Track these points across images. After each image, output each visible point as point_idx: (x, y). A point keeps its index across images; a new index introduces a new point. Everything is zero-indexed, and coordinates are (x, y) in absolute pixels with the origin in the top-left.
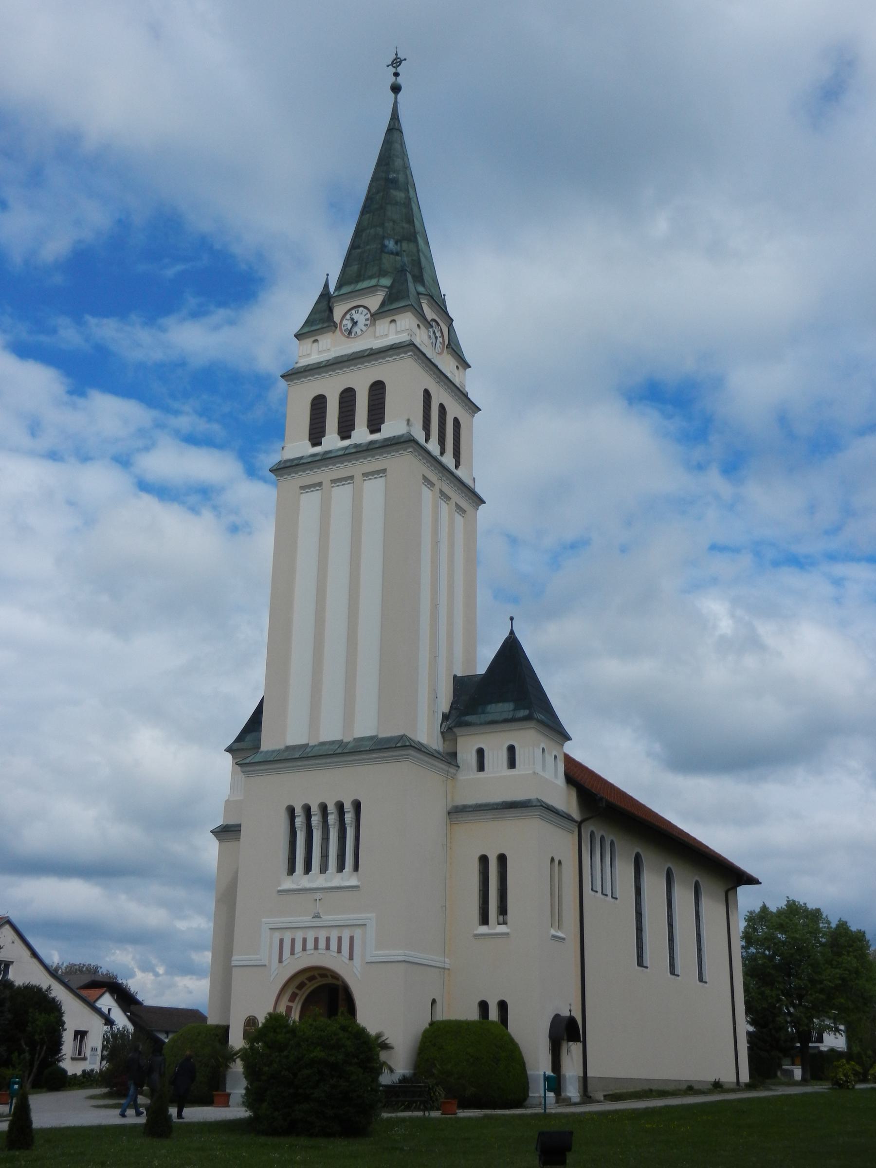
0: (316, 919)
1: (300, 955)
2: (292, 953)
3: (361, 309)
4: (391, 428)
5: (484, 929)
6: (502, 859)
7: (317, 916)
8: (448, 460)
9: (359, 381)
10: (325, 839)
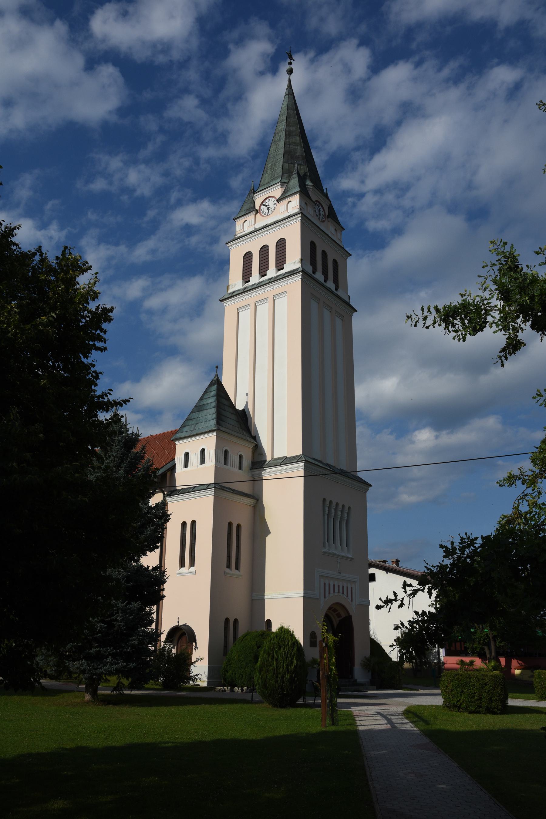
2: (329, 593)
3: (271, 199)
4: (288, 267)
5: (228, 571)
6: (194, 523)
7: (340, 573)
8: (330, 284)
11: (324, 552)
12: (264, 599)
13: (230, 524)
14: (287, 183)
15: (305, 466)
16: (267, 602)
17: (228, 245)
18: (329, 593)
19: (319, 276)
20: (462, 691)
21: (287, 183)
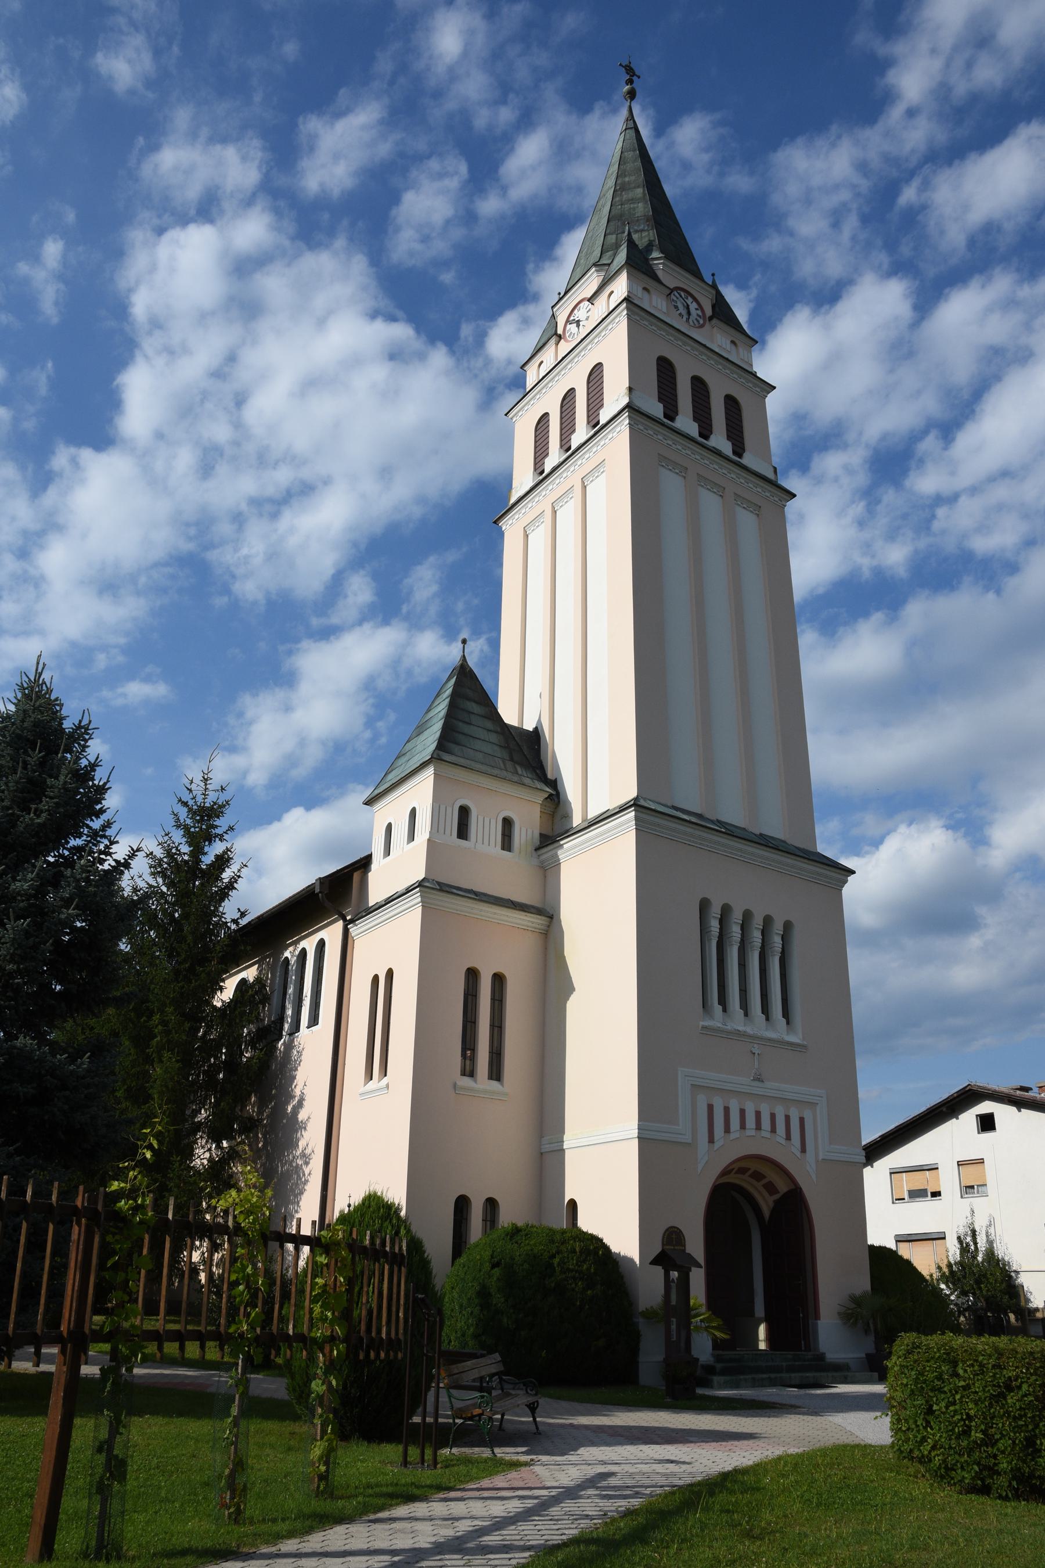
0: (757, 1083)
1: (737, 1135)
2: (727, 1130)
3: (581, 305)
5: (466, 1081)
6: (390, 974)
7: (759, 1079)
8: (720, 441)
10: (743, 965)
11: (703, 1027)
12: (563, 1150)
13: (472, 975)
14: (609, 265)
15: (637, 818)
16: (569, 1157)
17: (511, 415)
18: (727, 1130)
19: (686, 423)
20: (930, 1411)
21: (609, 265)
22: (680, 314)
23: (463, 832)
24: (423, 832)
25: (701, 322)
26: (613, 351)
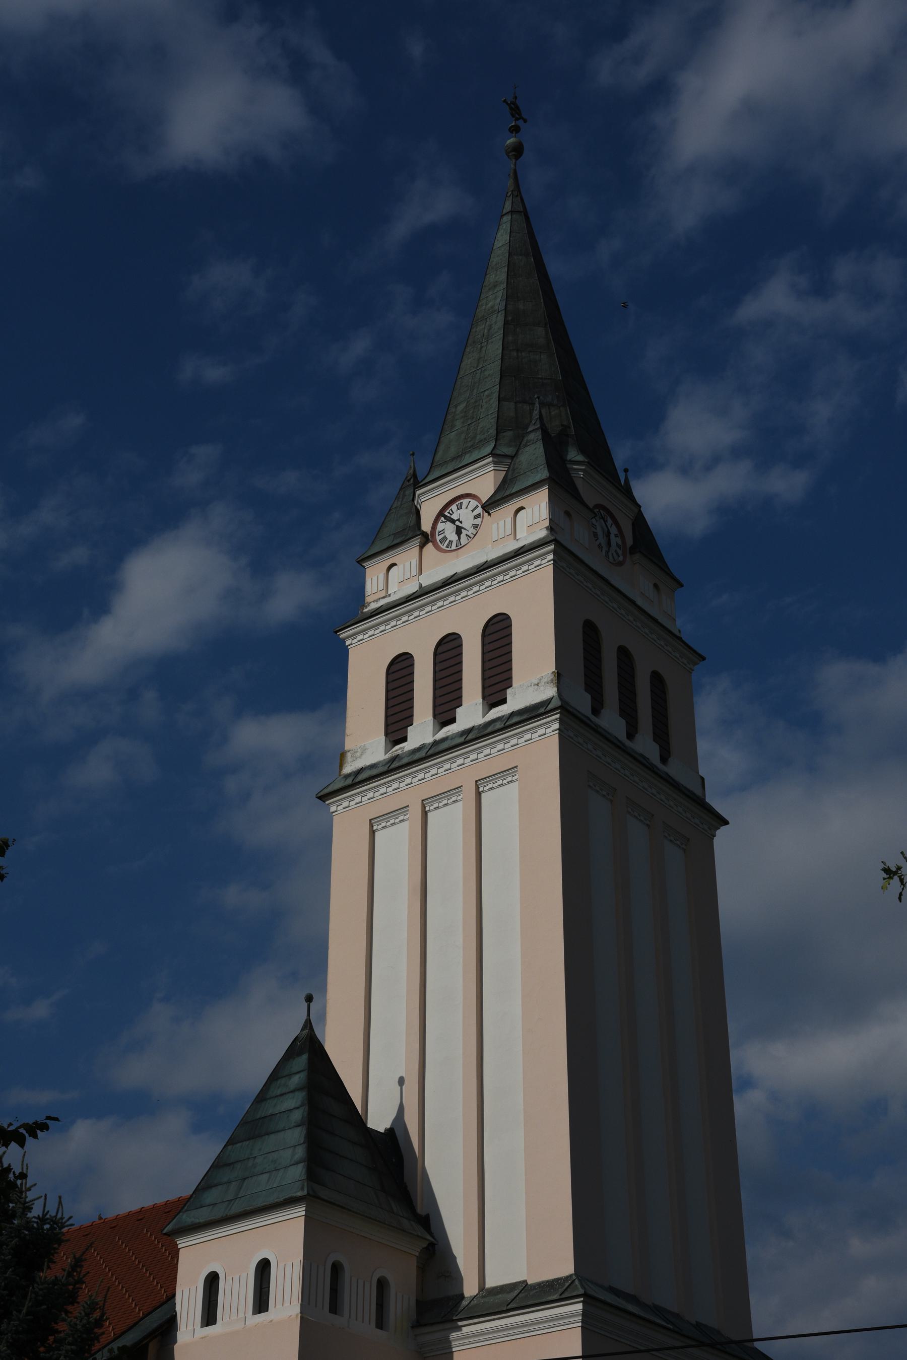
3: (465, 501)
4: (519, 697)
8: (645, 745)
9: (466, 618)
14: (512, 457)
15: (585, 1314)
21: (512, 457)
22: (600, 546)
23: (335, 1308)
24: (287, 1303)
25: (621, 558)
26: (531, 602)
